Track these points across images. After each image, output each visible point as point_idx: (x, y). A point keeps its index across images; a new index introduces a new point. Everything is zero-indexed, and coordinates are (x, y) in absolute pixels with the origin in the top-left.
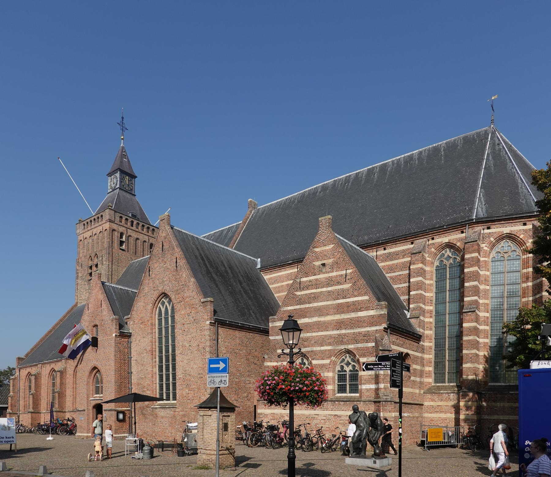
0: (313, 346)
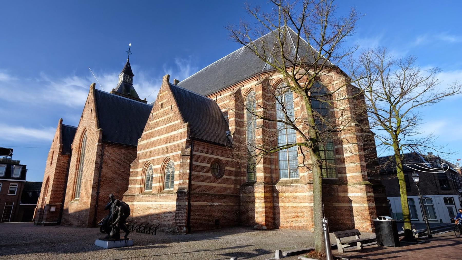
0: (154, 156)
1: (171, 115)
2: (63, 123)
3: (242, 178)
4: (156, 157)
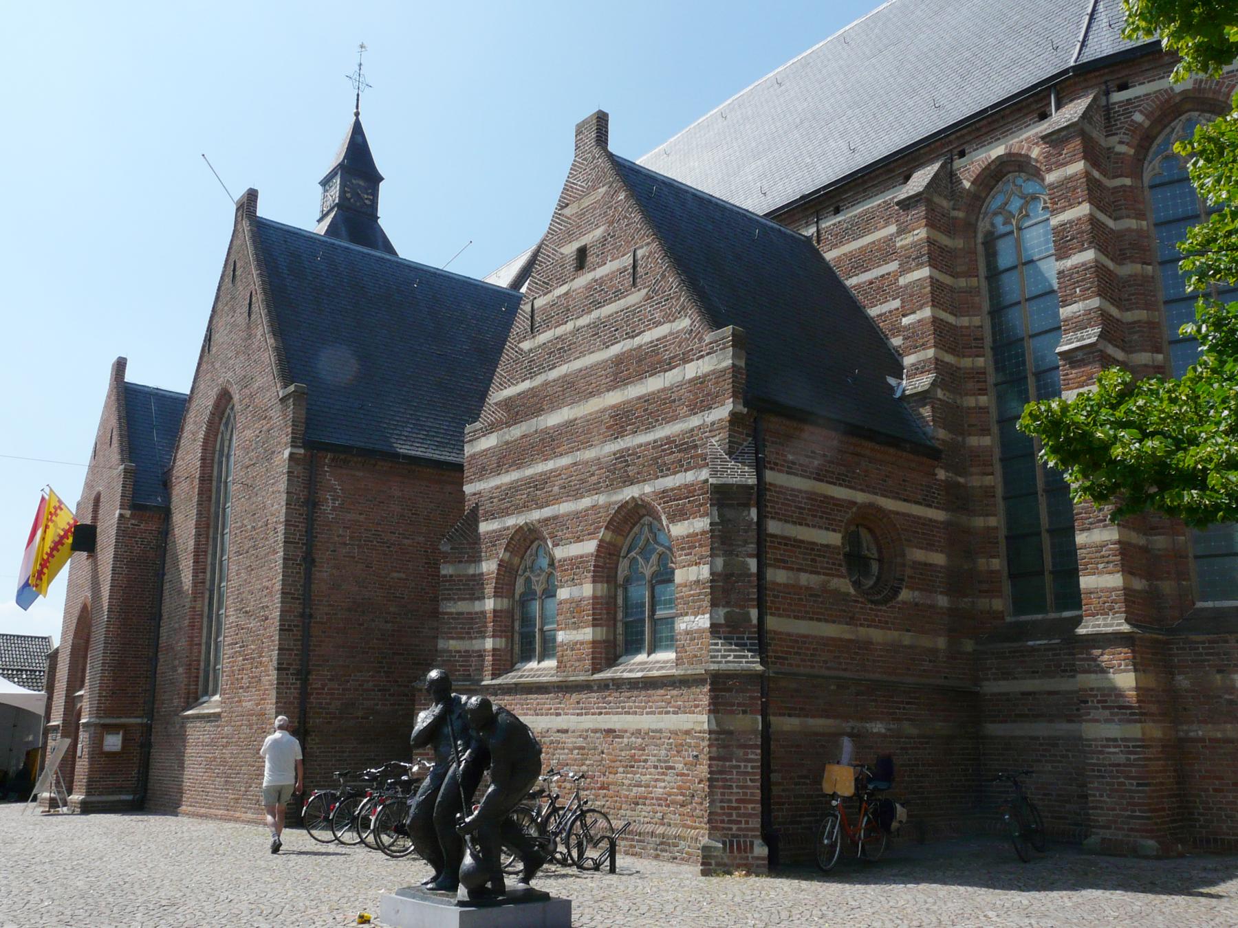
0: (557, 500)
1: (635, 298)
2: (131, 377)
3: (983, 603)
4: (565, 507)
